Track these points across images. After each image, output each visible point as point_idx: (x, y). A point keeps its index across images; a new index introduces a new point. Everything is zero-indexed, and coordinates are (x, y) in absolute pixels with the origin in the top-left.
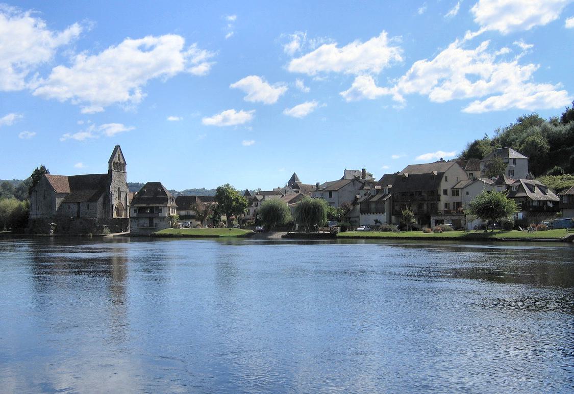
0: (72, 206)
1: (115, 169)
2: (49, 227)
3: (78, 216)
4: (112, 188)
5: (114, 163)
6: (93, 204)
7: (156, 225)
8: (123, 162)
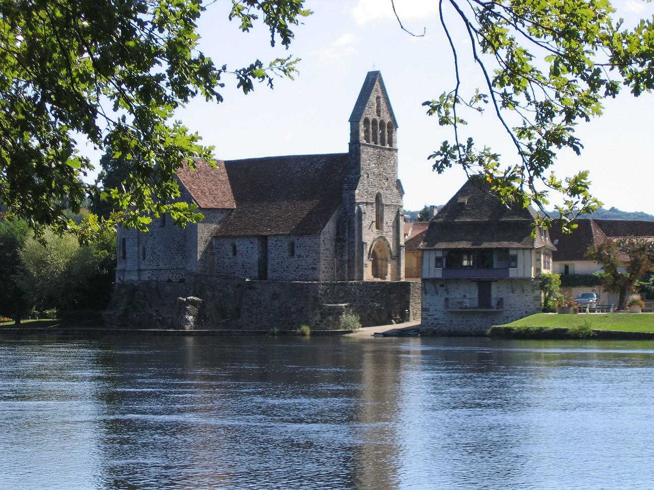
0: (242, 246)
1: (367, 138)
2: (181, 309)
3: (263, 274)
4: (360, 195)
5: (366, 121)
6: (307, 240)
7: (500, 302)
8: (387, 120)
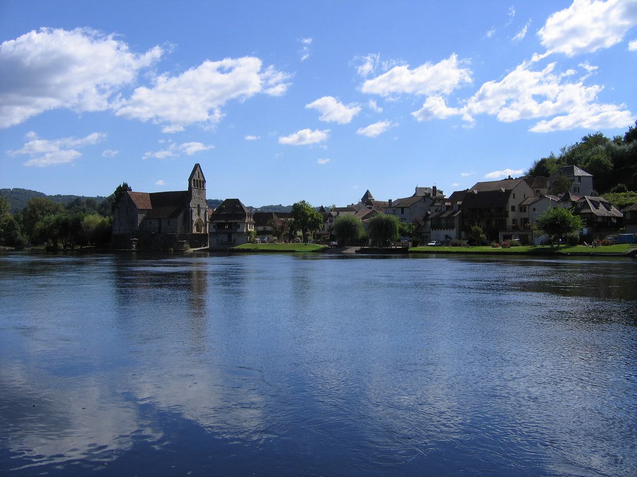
2: (131, 243)
4: (192, 204)
5: (194, 180)
7: (235, 240)
8: (202, 180)
